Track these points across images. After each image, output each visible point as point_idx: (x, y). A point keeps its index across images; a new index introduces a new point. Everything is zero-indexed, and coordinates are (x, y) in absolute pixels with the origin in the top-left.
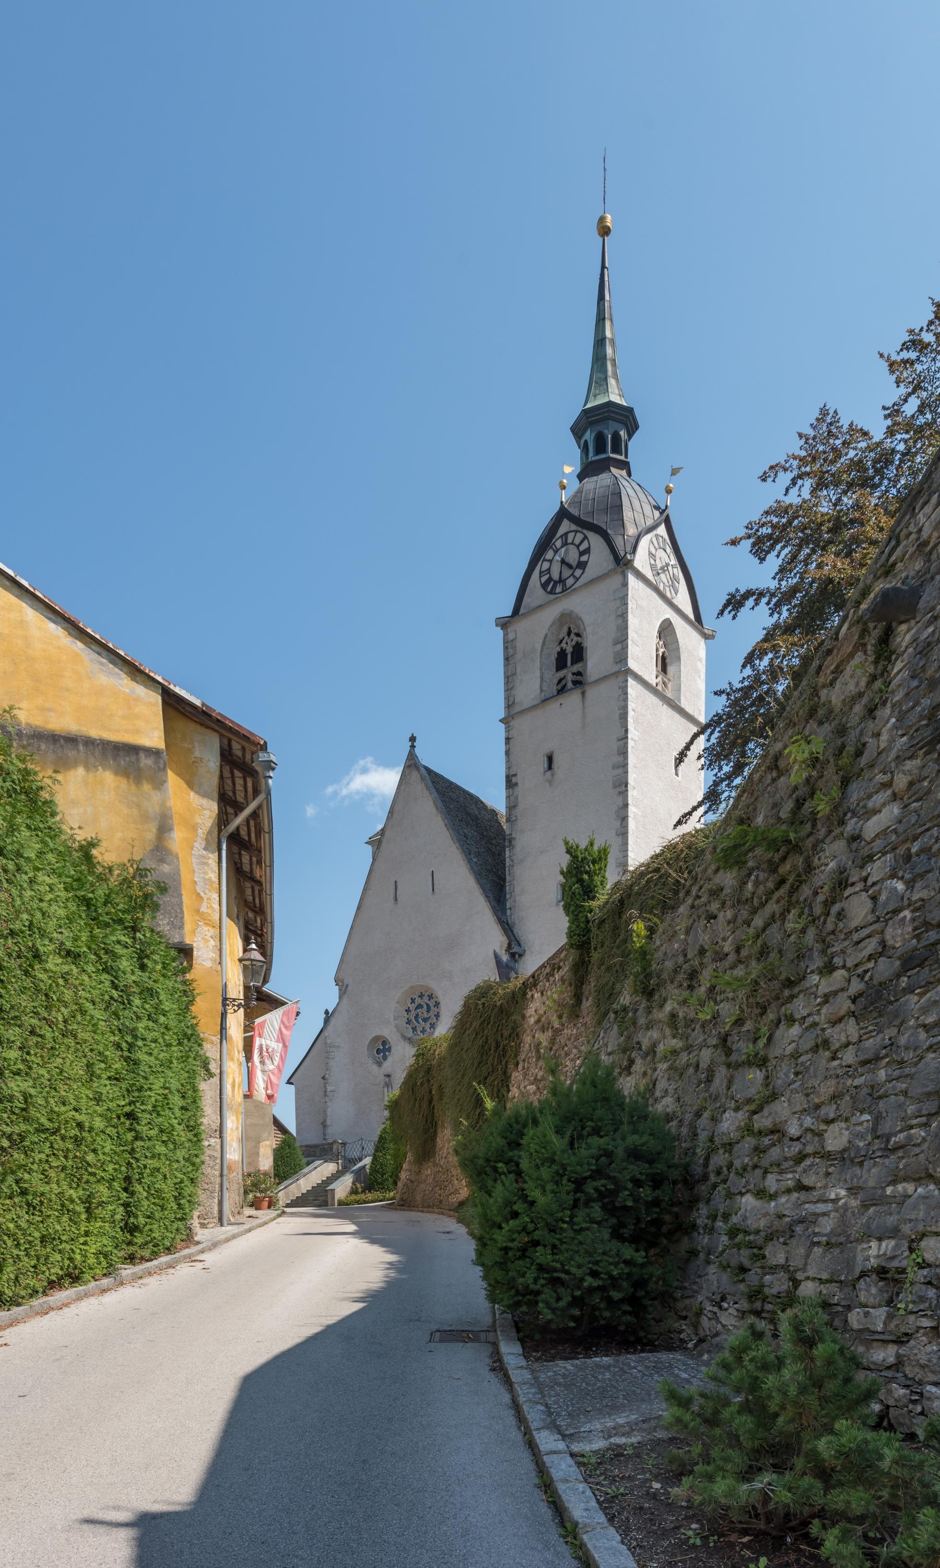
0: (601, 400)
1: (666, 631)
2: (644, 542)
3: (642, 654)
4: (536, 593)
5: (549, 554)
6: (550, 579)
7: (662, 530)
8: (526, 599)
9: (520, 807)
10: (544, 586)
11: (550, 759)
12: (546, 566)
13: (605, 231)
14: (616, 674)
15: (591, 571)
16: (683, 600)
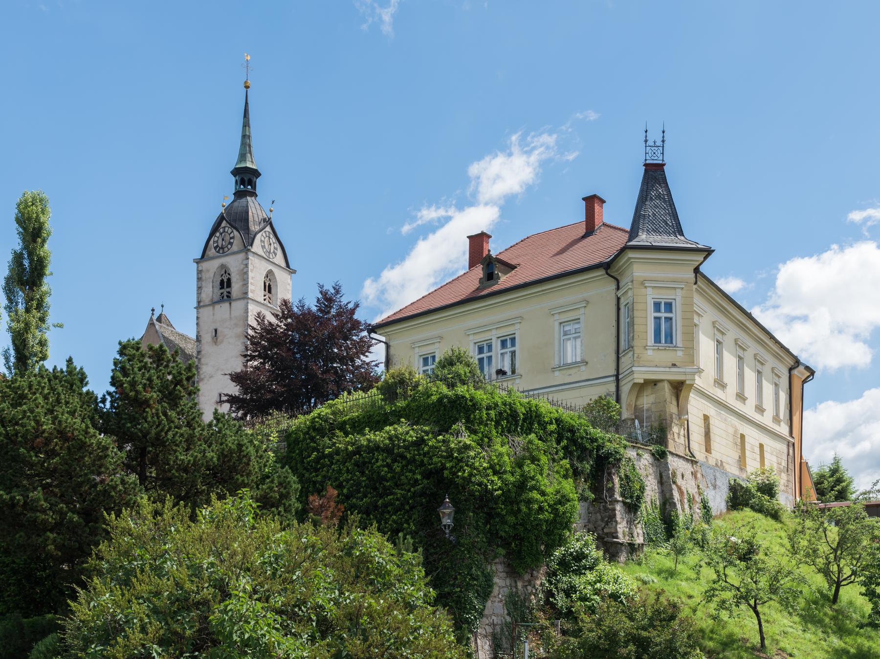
0: (242, 165)
1: (269, 274)
2: (259, 236)
3: (256, 290)
4: (212, 252)
5: (218, 234)
6: (217, 246)
7: (268, 229)
8: (208, 252)
9: (203, 353)
10: (215, 248)
11: (216, 330)
12: (216, 239)
13: (247, 87)
14: (244, 298)
15: (235, 248)
16: (279, 259)
